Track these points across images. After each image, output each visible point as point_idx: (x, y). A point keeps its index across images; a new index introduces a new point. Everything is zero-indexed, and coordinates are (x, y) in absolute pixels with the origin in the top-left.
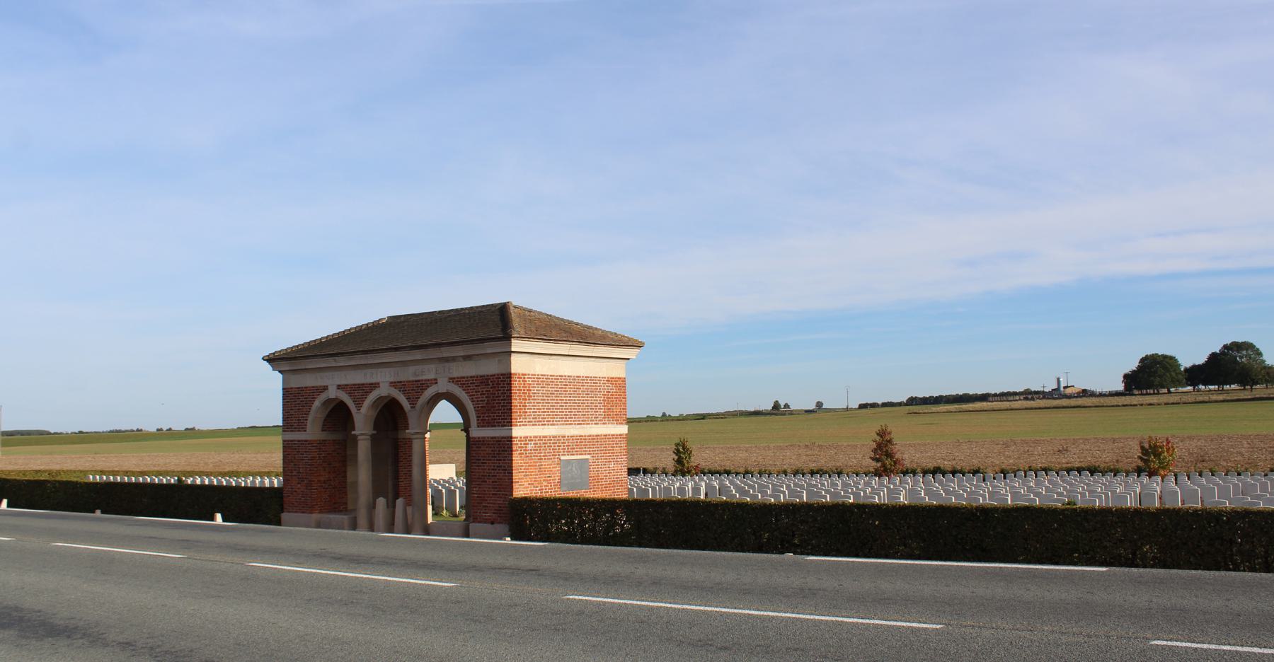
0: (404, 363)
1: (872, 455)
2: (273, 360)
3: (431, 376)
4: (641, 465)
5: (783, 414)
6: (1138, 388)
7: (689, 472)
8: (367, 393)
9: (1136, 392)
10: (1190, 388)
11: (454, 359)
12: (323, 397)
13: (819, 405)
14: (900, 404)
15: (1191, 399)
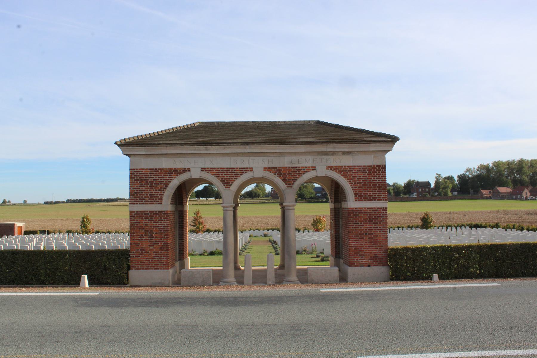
0: (281, 154)
1: (193, 224)
2: (123, 145)
3: (309, 164)
4: (46, 229)
7: (89, 232)
8: (171, 178)
10: (196, 199)
11: (333, 153)
12: (184, 177)
13: (25, 201)
14: (63, 202)
15: (196, 203)
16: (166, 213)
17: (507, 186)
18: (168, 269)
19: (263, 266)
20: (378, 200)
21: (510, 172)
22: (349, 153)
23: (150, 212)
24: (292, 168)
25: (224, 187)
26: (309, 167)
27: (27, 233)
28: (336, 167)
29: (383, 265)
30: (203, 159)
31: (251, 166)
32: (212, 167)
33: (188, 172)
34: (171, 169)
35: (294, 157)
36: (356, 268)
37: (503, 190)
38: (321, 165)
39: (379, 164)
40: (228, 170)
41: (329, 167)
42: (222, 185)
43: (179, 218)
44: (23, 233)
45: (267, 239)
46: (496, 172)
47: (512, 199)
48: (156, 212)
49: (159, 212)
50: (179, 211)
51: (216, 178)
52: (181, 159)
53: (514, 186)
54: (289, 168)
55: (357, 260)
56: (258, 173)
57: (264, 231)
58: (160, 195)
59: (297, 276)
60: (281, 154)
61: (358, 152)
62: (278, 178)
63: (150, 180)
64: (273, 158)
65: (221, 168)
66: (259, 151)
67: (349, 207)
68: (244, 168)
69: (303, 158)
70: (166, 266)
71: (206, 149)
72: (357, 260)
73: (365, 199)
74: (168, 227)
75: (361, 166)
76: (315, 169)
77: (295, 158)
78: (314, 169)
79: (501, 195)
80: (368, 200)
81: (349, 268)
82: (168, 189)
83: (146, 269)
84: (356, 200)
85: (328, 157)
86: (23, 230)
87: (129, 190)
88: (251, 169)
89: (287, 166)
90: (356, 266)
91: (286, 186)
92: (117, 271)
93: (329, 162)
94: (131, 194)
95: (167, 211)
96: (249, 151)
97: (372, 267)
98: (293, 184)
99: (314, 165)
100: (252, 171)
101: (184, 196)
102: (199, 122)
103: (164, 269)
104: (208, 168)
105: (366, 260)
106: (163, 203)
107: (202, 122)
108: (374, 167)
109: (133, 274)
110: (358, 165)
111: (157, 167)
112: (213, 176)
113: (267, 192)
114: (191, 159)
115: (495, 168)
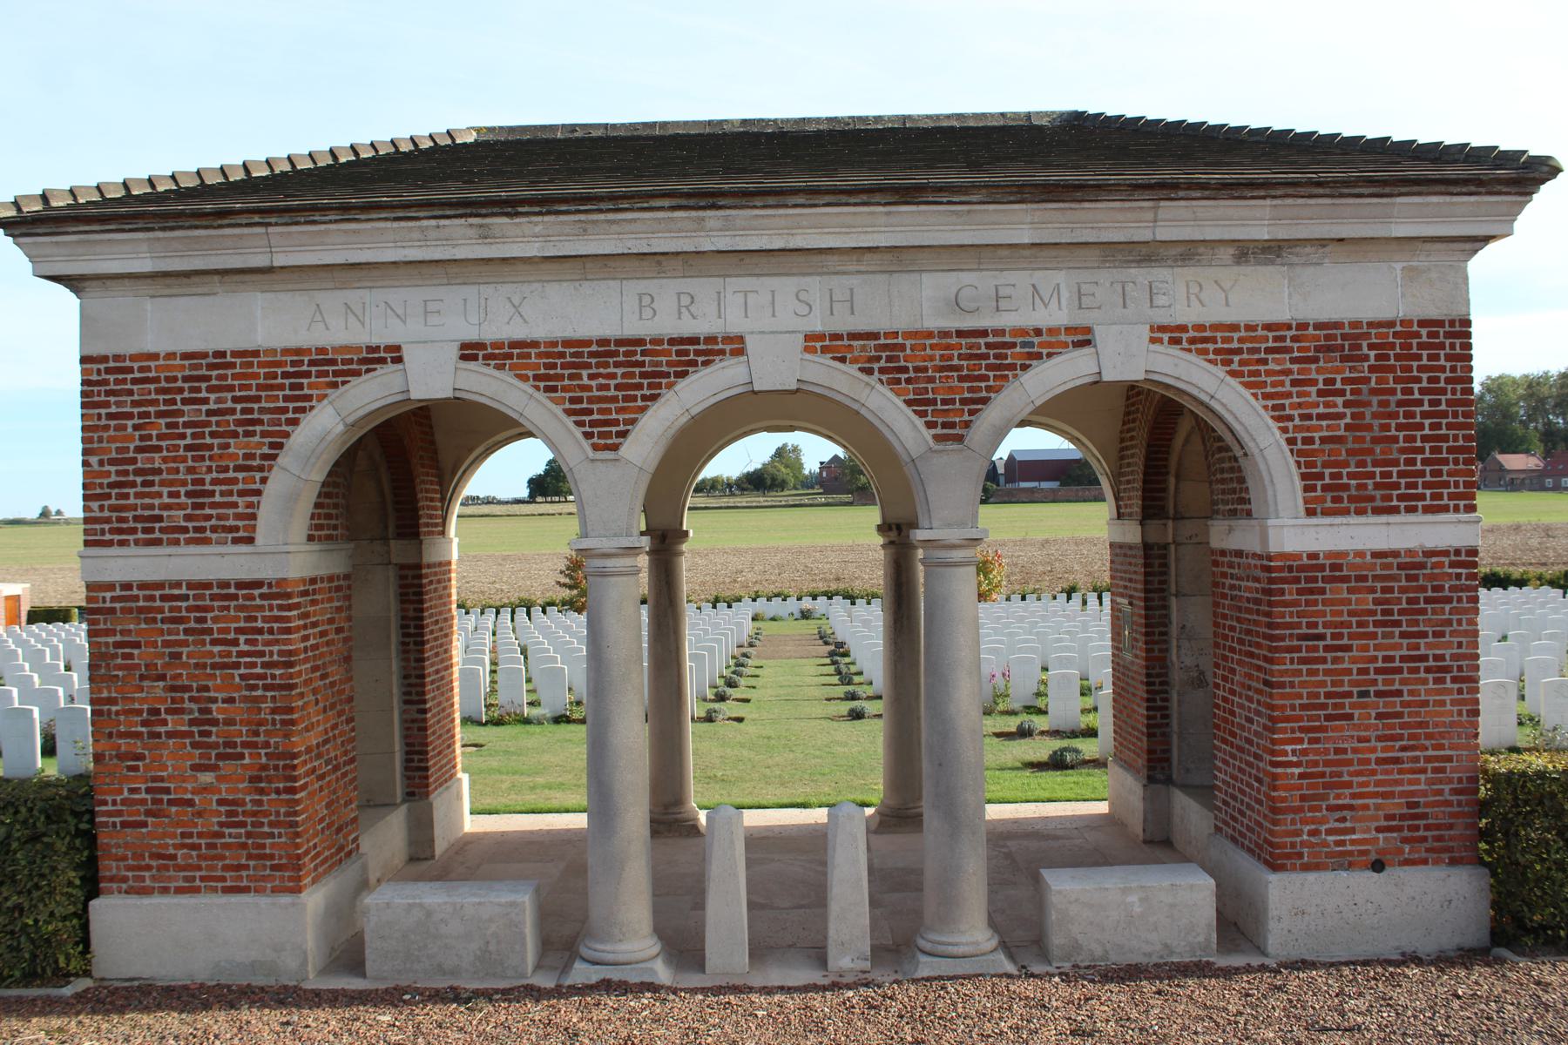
0: (900, 258)
1: (564, 580)
3: (1055, 315)
5: (56, 523)
6: (544, 494)
8: (302, 403)
9: (539, 499)
11: (1188, 252)
12: (369, 395)
16: (278, 591)
17: (1527, 452)
18: (299, 890)
19: (804, 806)
20: (1428, 510)
21: (1535, 409)
22: (1272, 251)
23: (191, 585)
24: (960, 334)
25: (586, 444)
26: (1051, 331)
27: (37, 616)
28: (1200, 327)
29: (1454, 862)
30: (470, 292)
31: (733, 329)
32: (519, 332)
33: (391, 367)
34: (298, 351)
35: (967, 278)
36: (1311, 877)
37: (1514, 462)
38: (1129, 311)
39: (1433, 313)
40: (606, 349)
41: (1162, 329)
42: (578, 432)
43: (403, 598)
44: (24, 618)
45: (810, 627)
46: (1494, 408)
47: (1543, 489)
48: (224, 584)
49: (241, 585)
50: (402, 567)
51: (541, 396)
52: (353, 296)
53: (1547, 454)
54: (945, 334)
55: (1313, 833)
56: (775, 364)
57: (799, 599)
58: (242, 493)
59: (992, 924)
60: (900, 258)
61: (1322, 242)
62: (885, 390)
63: (189, 413)
64: (854, 281)
65: (568, 343)
66: (778, 244)
67: (1274, 548)
68: (694, 340)
69: (1019, 280)
70: (287, 876)
71: (485, 236)
72: (1313, 833)
73: (1362, 504)
74: (291, 665)
75: (1338, 325)
76: (1087, 343)
77: (976, 282)
78: (1083, 338)
79: (1508, 477)
80: (1378, 511)
81: (1274, 878)
82: (284, 459)
83: (180, 891)
84: (1310, 513)
85: (1159, 274)
86: (25, 608)
87: (79, 470)
88: (736, 346)
89: (933, 323)
90: (1306, 868)
91: (928, 434)
92: (19, 908)
93: (1161, 300)
94: (90, 495)
95: (281, 582)
96: (723, 244)
97: (1394, 874)
98: (967, 425)
99: (1081, 319)
100: (740, 352)
101: (426, 490)
102: (478, 130)
103: (275, 890)
104: (496, 345)
105: (1364, 834)
106: (260, 538)
107: (491, 130)
108: (1405, 330)
109: (113, 916)
110: (1324, 317)
111: (227, 345)
112: (527, 387)
113: (806, 472)
114: (408, 296)
115: (1488, 397)
